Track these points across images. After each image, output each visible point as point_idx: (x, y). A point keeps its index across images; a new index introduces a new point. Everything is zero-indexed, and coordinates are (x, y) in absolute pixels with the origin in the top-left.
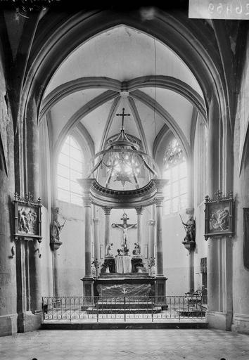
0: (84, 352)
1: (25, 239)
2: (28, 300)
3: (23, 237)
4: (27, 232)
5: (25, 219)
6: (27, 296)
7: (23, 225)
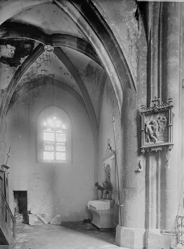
0: (111, 38)
1: (153, 150)
2: (157, 217)
3: (150, 148)
4: (155, 142)
5: (152, 128)
6: (157, 212)
7: (150, 135)
